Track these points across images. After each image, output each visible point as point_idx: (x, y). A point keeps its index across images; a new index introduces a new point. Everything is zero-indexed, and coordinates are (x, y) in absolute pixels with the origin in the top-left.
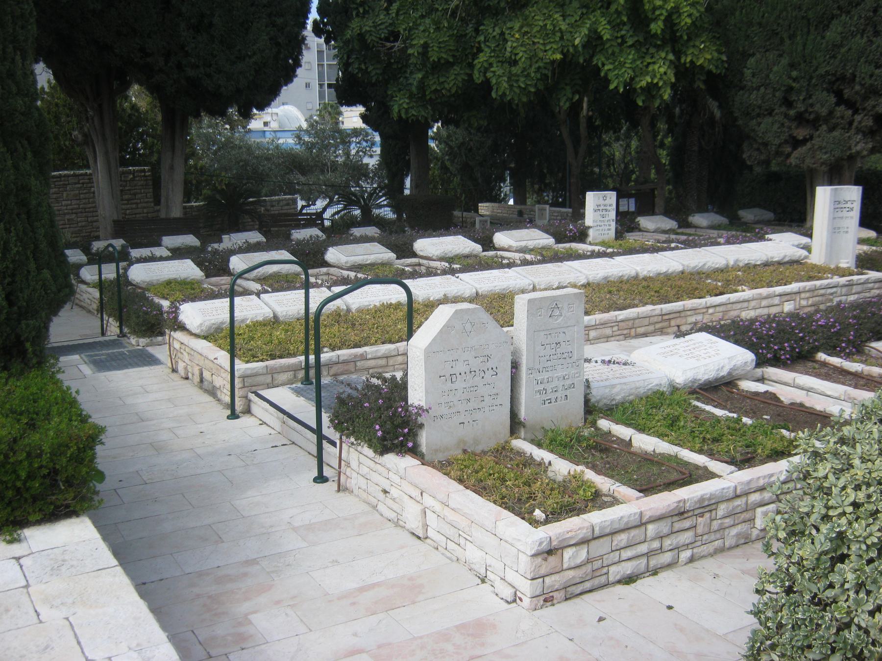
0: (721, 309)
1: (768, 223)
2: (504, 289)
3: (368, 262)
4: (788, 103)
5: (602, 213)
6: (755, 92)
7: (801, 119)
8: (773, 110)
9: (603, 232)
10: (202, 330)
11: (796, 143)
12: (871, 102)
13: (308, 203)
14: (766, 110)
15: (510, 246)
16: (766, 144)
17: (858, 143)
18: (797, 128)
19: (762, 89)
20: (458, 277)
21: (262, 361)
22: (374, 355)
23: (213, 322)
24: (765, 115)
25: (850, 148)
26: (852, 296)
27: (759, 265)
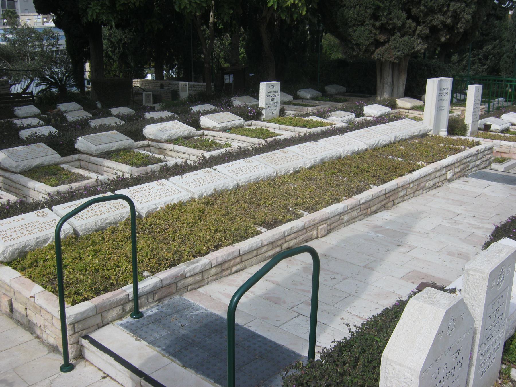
0: (416, 183)
1: (343, 94)
2: (257, 179)
3: (114, 149)
4: (375, 17)
5: (271, 98)
6: (352, 9)
7: (383, 29)
8: (365, 22)
9: (272, 112)
10: (5, 258)
11: (378, 44)
12: (430, 18)
13: (14, 82)
14: (360, 21)
15: (214, 127)
16: (358, 45)
17: (419, 44)
18: (380, 34)
19: (358, 7)
20: (215, 170)
21: (87, 299)
22: (192, 273)
23: (15, 247)
24: (358, 25)
25: (413, 48)
26: (478, 161)
27: (408, 139)
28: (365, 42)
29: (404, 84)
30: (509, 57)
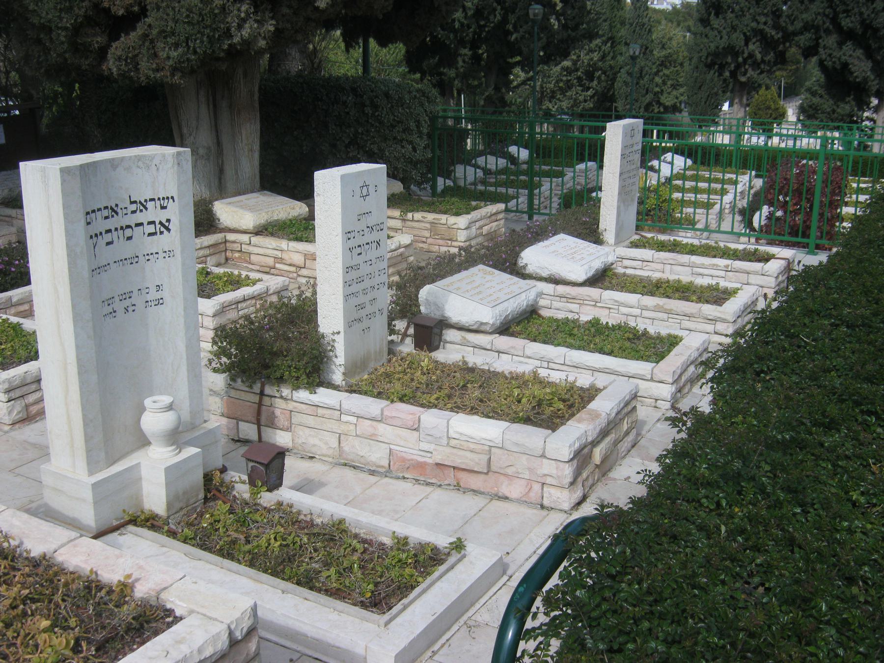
17: (244, 20)
25: (228, 34)
28: (61, 19)
29: (251, 150)
30: (629, 74)
